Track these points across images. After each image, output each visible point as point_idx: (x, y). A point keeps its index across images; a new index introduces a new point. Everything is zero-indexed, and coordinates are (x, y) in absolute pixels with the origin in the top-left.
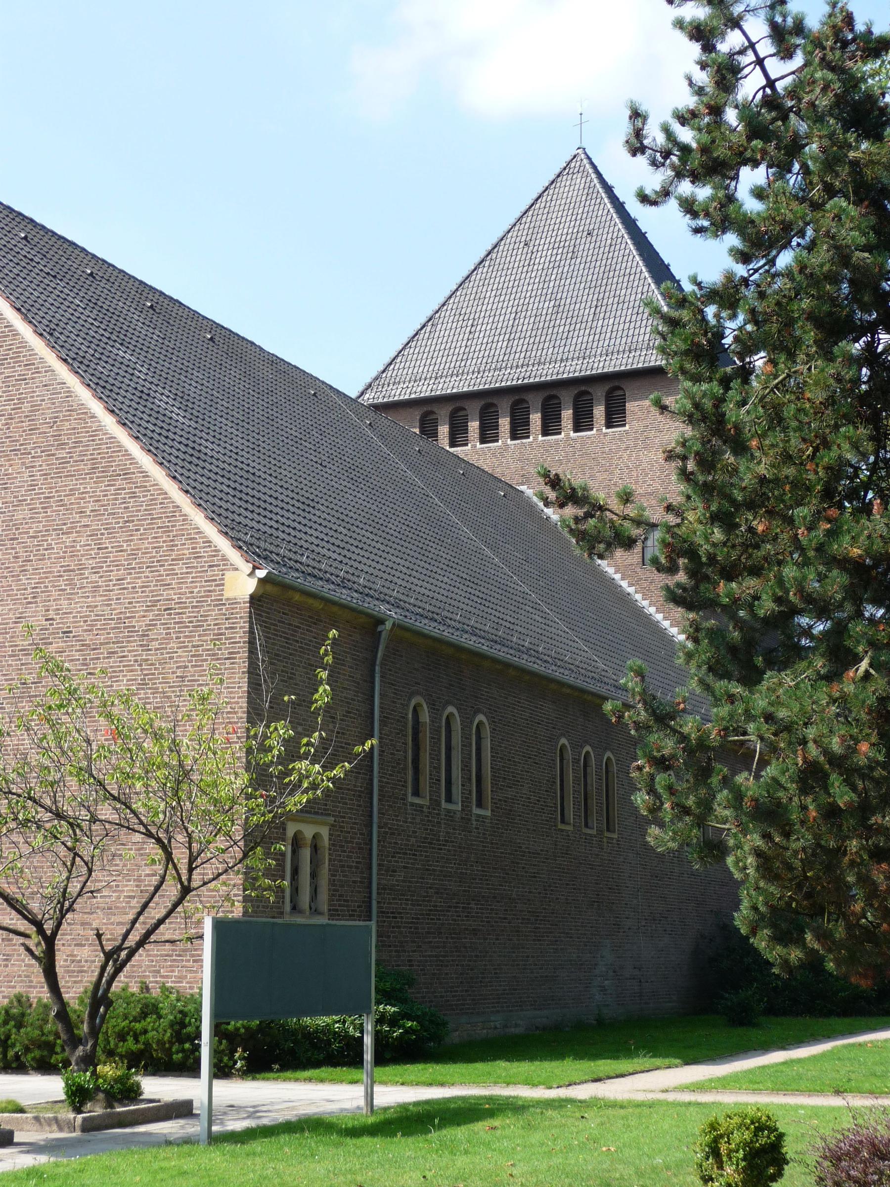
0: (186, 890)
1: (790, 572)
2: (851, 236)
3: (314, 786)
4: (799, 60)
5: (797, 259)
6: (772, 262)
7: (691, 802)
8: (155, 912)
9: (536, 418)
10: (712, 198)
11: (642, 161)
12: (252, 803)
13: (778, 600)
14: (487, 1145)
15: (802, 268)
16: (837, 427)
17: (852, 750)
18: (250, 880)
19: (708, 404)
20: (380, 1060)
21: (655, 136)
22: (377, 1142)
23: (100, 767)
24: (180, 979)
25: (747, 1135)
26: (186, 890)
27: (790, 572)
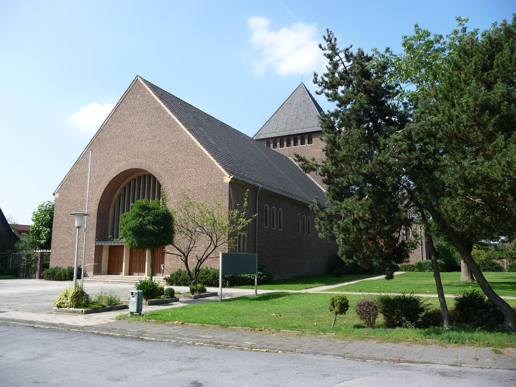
0: (216, 247)
1: (350, 176)
2: (364, 101)
3: (244, 224)
4: (351, 62)
5: (351, 106)
6: (346, 107)
7: (328, 227)
8: (209, 251)
9: (292, 142)
10: (332, 93)
11: (317, 85)
12: (230, 228)
13: (348, 183)
14: (282, 303)
15: (353, 108)
16: (361, 144)
17: (364, 216)
18: (230, 244)
19: (332, 139)
20: (258, 284)
21: (319, 79)
22: (258, 302)
23: (197, 220)
24: (214, 266)
25: (340, 301)
26: (216, 247)
27: (350, 176)
